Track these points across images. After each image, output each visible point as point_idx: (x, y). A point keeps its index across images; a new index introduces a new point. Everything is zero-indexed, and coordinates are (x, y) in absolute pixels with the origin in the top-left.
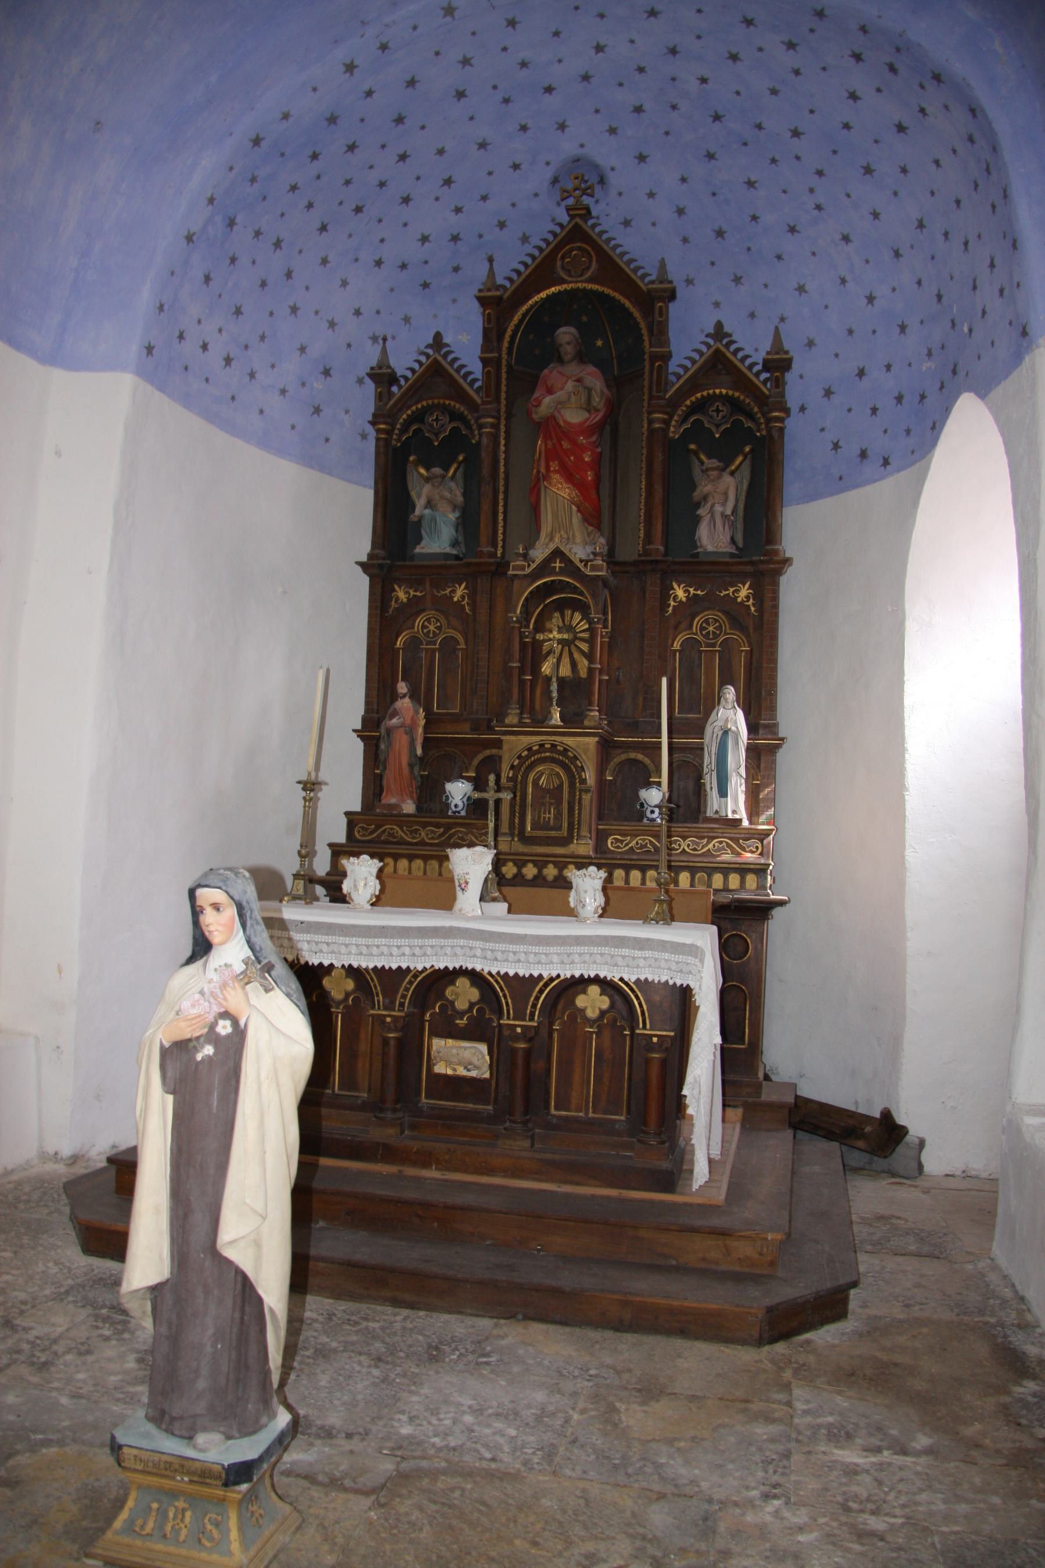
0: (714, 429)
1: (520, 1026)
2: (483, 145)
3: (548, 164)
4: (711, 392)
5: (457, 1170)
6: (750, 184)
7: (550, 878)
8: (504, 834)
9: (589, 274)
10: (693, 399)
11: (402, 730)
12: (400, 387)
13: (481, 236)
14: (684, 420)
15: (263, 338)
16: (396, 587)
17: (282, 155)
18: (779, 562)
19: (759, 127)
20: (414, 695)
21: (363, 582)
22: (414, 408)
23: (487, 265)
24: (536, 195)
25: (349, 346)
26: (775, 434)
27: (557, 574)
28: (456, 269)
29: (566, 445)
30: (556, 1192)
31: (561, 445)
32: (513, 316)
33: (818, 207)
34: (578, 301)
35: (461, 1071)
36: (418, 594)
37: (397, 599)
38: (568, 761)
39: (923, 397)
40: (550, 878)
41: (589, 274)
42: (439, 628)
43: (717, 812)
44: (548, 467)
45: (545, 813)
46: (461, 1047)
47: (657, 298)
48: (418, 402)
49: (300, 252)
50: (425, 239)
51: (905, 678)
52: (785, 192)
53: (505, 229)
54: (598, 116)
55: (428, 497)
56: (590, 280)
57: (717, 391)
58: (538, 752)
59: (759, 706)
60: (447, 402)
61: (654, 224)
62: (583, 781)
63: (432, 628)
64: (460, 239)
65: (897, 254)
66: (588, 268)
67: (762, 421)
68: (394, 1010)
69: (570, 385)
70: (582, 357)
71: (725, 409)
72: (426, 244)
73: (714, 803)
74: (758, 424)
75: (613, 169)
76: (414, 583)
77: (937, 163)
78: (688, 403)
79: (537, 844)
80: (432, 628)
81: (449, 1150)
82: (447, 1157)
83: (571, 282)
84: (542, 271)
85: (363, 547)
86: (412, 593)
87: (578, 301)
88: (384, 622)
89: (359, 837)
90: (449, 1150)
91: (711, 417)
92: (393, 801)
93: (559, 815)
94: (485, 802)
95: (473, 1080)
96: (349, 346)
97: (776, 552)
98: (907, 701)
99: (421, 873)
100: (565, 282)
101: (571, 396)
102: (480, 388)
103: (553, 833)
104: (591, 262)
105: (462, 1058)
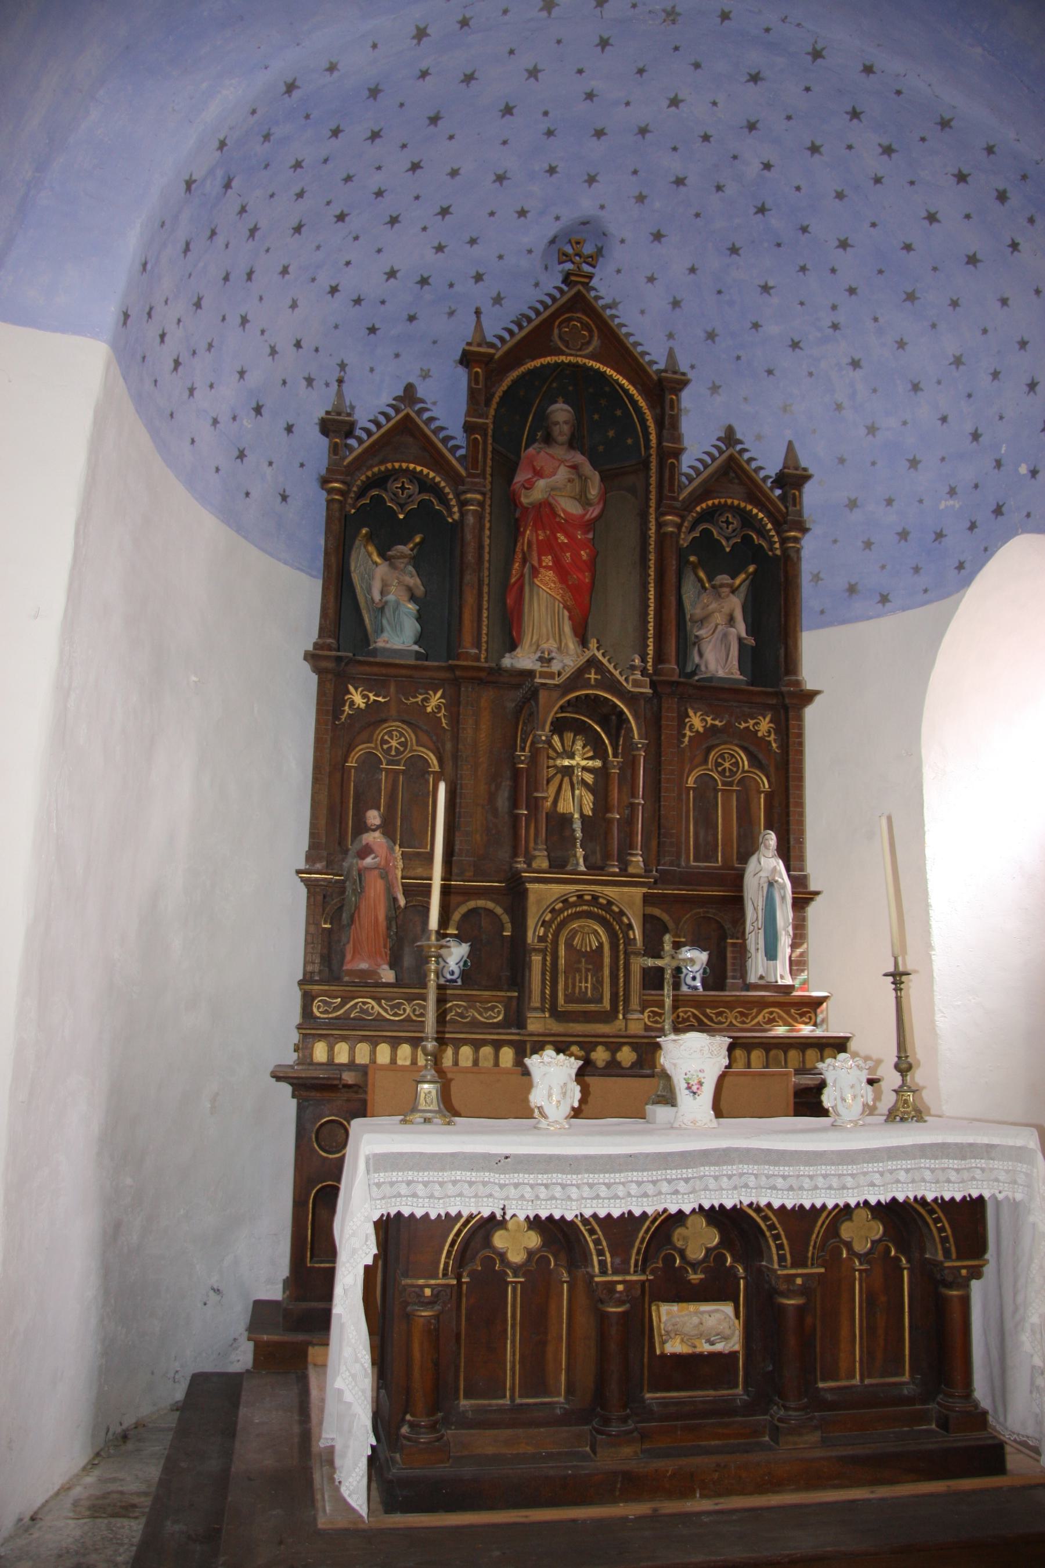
0: (724, 543)
1: (799, 1274)
2: (500, 179)
3: (557, 218)
4: (723, 501)
5: (729, 1492)
6: (766, 289)
7: (600, 1064)
8: (535, 1009)
9: (591, 349)
10: (704, 505)
11: (376, 872)
12: (360, 441)
13: (451, 285)
14: (692, 529)
15: (210, 346)
16: (351, 688)
17: (307, 117)
18: (792, 695)
19: (804, 230)
20: (387, 828)
21: (306, 683)
22: (376, 469)
23: (474, 317)
24: (530, 252)
25: (284, 383)
26: (793, 555)
27: (592, 687)
28: (412, 318)
29: (562, 538)
30: (869, 1500)
31: (556, 538)
32: (501, 380)
33: (835, 327)
34: (567, 378)
35: (706, 1348)
36: (380, 699)
37: (352, 703)
38: (609, 916)
39: (939, 535)
40: (600, 1064)
41: (591, 349)
42: (404, 744)
43: (761, 977)
44: (540, 561)
45: (580, 982)
46: (703, 1313)
47: (664, 389)
48: (382, 462)
49: (267, 251)
50: (392, 274)
51: (926, 829)
52: (802, 304)
53: (481, 283)
54: (634, 178)
55: (382, 580)
56: (592, 357)
57: (729, 501)
58: (574, 905)
59: (790, 852)
60: (419, 468)
61: (642, 312)
62: (629, 942)
63: (394, 743)
64: (429, 284)
65: (916, 388)
66: (589, 343)
67: (776, 539)
68: (628, 1273)
69: (562, 474)
70: (572, 444)
71: (736, 523)
72: (392, 280)
73: (757, 967)
74: (771, 543)
75: (622, 241)
76: (371, 684)
77: (1004, 302)
78: (698, 509)
79: (574, 1021)
80: (394, 743)
81: (718, 1465)
82: (716, 1476)
83: (571, 355)
84: (537, 335)
85: (308, 634)
86: (372, 697)
87: (567, 378)
88: (337, 733)
89: (318, 1015)
90: (718, 1465)
91: (721, 528)
92: (364, 966)
93: (599, 983)
94: (661, 970)
95: (719, 1355)
96: (284, 383)
97: (798, 683)
98: (928, 852)
99: (469, 1064)
100: (562, 353)
101: (557, 480)
102: (464, 457)
103: (592, 1007)
104: (591, 337)
105: (702, 1327)
